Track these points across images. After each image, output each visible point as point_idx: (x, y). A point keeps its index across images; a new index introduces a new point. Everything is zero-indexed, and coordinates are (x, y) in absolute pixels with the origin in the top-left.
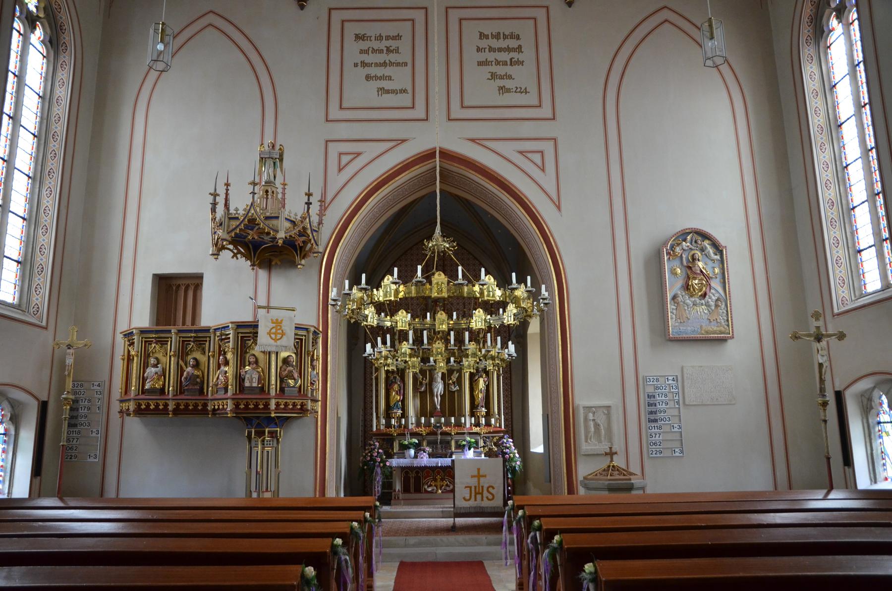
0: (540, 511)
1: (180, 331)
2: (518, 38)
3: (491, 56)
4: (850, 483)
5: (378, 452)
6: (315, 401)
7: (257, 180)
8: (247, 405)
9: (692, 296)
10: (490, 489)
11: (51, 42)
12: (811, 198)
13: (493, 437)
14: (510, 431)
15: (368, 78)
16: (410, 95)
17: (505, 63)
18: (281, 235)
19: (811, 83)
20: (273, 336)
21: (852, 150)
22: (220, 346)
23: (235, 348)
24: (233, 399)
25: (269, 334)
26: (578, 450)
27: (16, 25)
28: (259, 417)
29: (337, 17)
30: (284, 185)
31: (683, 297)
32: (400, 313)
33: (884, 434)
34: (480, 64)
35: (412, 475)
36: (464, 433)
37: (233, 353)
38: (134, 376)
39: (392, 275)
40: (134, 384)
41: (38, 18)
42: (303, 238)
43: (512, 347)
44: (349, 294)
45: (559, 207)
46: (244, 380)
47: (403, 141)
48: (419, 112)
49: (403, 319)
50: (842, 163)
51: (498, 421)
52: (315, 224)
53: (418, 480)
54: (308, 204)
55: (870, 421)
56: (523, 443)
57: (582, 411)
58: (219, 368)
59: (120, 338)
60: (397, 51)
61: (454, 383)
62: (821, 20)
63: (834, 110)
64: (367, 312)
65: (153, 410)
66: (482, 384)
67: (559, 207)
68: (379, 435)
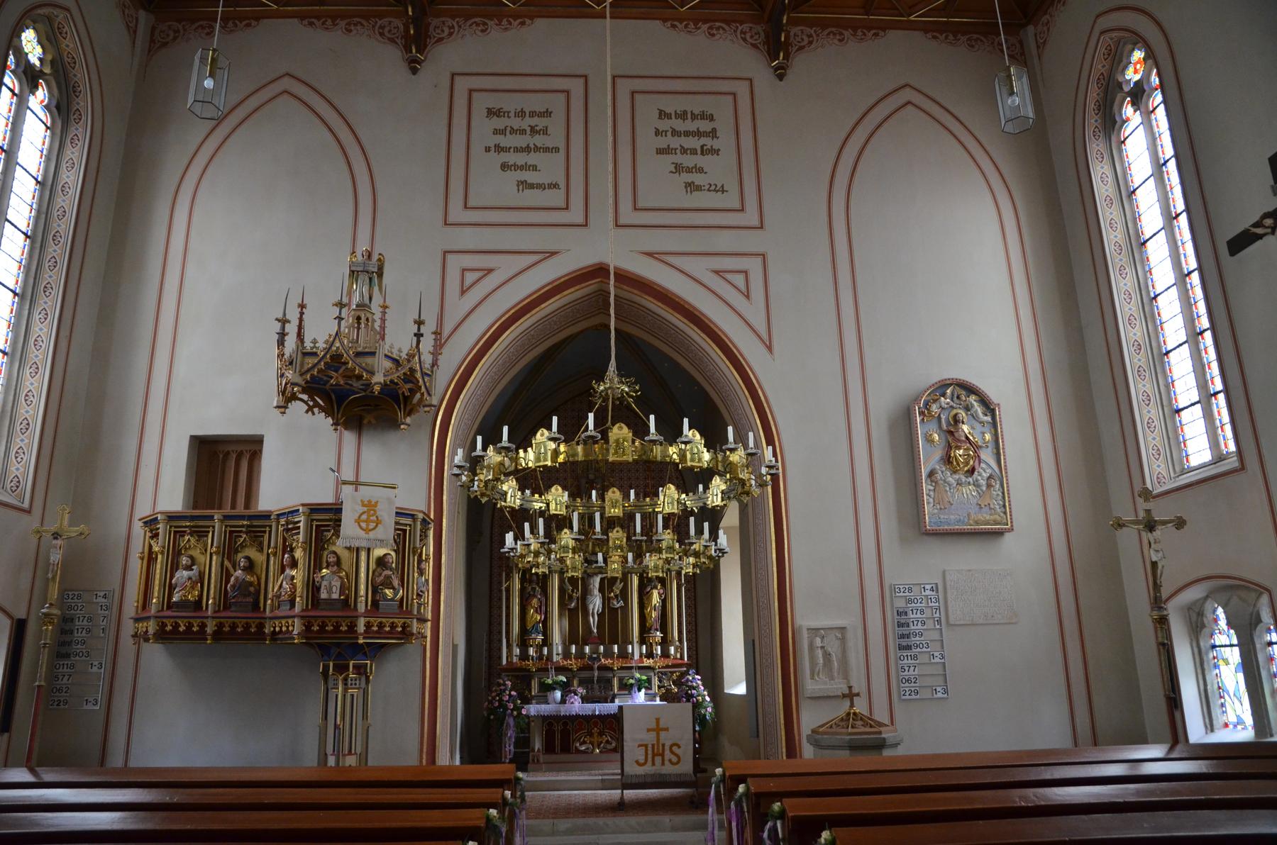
0: (772, 785)
1: (226, 517)
2: (711, 118)
3: (675, 142)
4: (1175, 733)
6: (422, 620)
7: (345, 300)
8: (323, 626)
9: (955, 472)
10: (675, 748)
11: (58, 107)
12: (1110, 340)
13: (672, 673)
14: (695, 664)
15: (504, 167)
17: (694, 152)
18: (379, 378)
19: (1103, 189)
20: (364, 525)
21: (1162, 275)
22: (285, 540)
23: (308, 542)
24: (302, 617)
25: (358, 521)
27: (7, 80)
28: (341, 642)
29: (462, 85)
30: (385, 307)
31: (944, 474)
32: (553, 489)
33: (1221, 662)
34: (660, 151)
35: (558, 728)
36: (631, 668)
37: (304, 550)
38: (157, 582)
39: (549, 428)
40: (156, 594)
41: (41, 74)
42: (409, 386)
44: (482, 457)
45: (770, 348)
46: (319, 589)
47: (553, 254)
48: (576, 215)
49: (557, 499)
50: (1148, 292)
51: (679, 651)
52: (427, 365)
53: (566, 735)
54: (419, 335)
55: (1202, 644)
56: (714, 681)
57: (805, 635)
58: (283, 571)
59: (138, 529)
60: (545, 131)
61: (616, 596)
62: (1111, 107)
63: (1135, 224)
64: (505, 487)
66: (656, 598)
67: (770, 348)
68: (511, 670)
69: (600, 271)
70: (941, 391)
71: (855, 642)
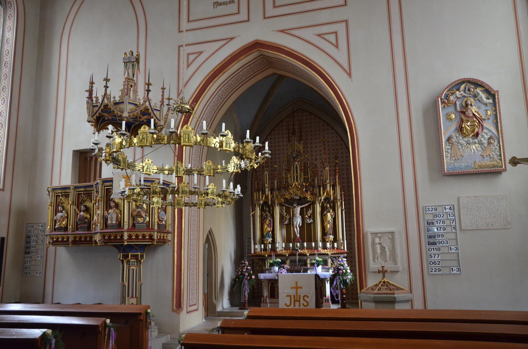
5: (247, 269)
10: (306, 298)
13: (339, 257)
16: (236, 4)
26: (367, 268)
36: (315, 254)
43: (239, 188)
45: (350, 75)
46: (107, 219)
47: (232, 39)
48: (243, 16)
65: (135, 239)
66: (329, 216)
67: (350, 75)
69: (256, 45)
70: (457, 87)
71: (400, 241)
